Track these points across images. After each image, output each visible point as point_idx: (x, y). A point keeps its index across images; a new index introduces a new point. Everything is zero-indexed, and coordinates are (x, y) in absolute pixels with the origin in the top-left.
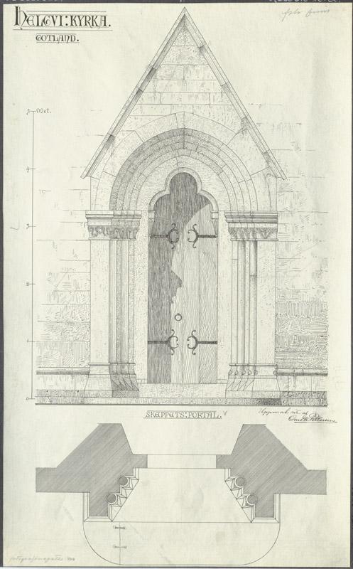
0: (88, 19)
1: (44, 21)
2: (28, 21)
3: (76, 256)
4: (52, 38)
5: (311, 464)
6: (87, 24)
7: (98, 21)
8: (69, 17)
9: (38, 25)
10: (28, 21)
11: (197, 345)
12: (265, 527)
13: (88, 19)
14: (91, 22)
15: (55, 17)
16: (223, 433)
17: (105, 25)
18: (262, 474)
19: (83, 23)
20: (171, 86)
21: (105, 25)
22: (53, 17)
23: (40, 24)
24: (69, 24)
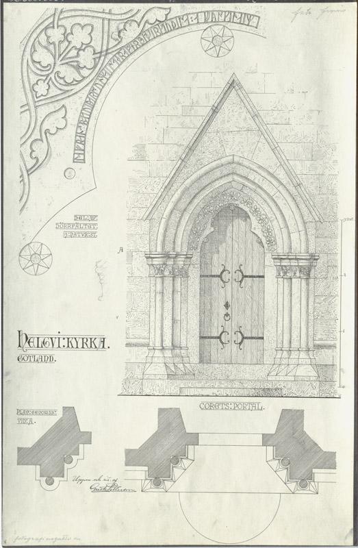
0: (85, 340)
1: (43, 343)
2: (29, 343)
3: (52, 539)
4: (32, 360)
5: (325, 447)
6: (85, 346)
7: (97, 342)
8: (66, 339)
9: (38, 347)
10: (29, 343)
11: (243, 278)
12: (304, 499)
13: (85, 340)
14: (89, 343)
15: (54, 339)
16: (268, 416)
17: (103, 347)
18: (296, 453)
19: (80, 345)
20: (74, 114)
21: (103, 347)
22: (51, 338)
23: (40, 346)
24: (66, 346)
